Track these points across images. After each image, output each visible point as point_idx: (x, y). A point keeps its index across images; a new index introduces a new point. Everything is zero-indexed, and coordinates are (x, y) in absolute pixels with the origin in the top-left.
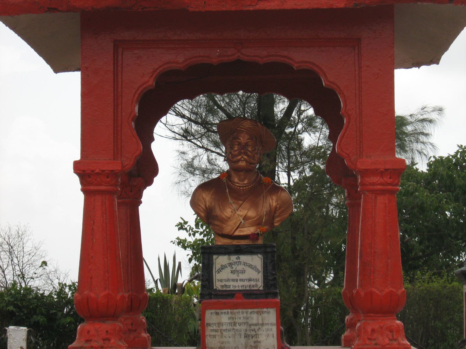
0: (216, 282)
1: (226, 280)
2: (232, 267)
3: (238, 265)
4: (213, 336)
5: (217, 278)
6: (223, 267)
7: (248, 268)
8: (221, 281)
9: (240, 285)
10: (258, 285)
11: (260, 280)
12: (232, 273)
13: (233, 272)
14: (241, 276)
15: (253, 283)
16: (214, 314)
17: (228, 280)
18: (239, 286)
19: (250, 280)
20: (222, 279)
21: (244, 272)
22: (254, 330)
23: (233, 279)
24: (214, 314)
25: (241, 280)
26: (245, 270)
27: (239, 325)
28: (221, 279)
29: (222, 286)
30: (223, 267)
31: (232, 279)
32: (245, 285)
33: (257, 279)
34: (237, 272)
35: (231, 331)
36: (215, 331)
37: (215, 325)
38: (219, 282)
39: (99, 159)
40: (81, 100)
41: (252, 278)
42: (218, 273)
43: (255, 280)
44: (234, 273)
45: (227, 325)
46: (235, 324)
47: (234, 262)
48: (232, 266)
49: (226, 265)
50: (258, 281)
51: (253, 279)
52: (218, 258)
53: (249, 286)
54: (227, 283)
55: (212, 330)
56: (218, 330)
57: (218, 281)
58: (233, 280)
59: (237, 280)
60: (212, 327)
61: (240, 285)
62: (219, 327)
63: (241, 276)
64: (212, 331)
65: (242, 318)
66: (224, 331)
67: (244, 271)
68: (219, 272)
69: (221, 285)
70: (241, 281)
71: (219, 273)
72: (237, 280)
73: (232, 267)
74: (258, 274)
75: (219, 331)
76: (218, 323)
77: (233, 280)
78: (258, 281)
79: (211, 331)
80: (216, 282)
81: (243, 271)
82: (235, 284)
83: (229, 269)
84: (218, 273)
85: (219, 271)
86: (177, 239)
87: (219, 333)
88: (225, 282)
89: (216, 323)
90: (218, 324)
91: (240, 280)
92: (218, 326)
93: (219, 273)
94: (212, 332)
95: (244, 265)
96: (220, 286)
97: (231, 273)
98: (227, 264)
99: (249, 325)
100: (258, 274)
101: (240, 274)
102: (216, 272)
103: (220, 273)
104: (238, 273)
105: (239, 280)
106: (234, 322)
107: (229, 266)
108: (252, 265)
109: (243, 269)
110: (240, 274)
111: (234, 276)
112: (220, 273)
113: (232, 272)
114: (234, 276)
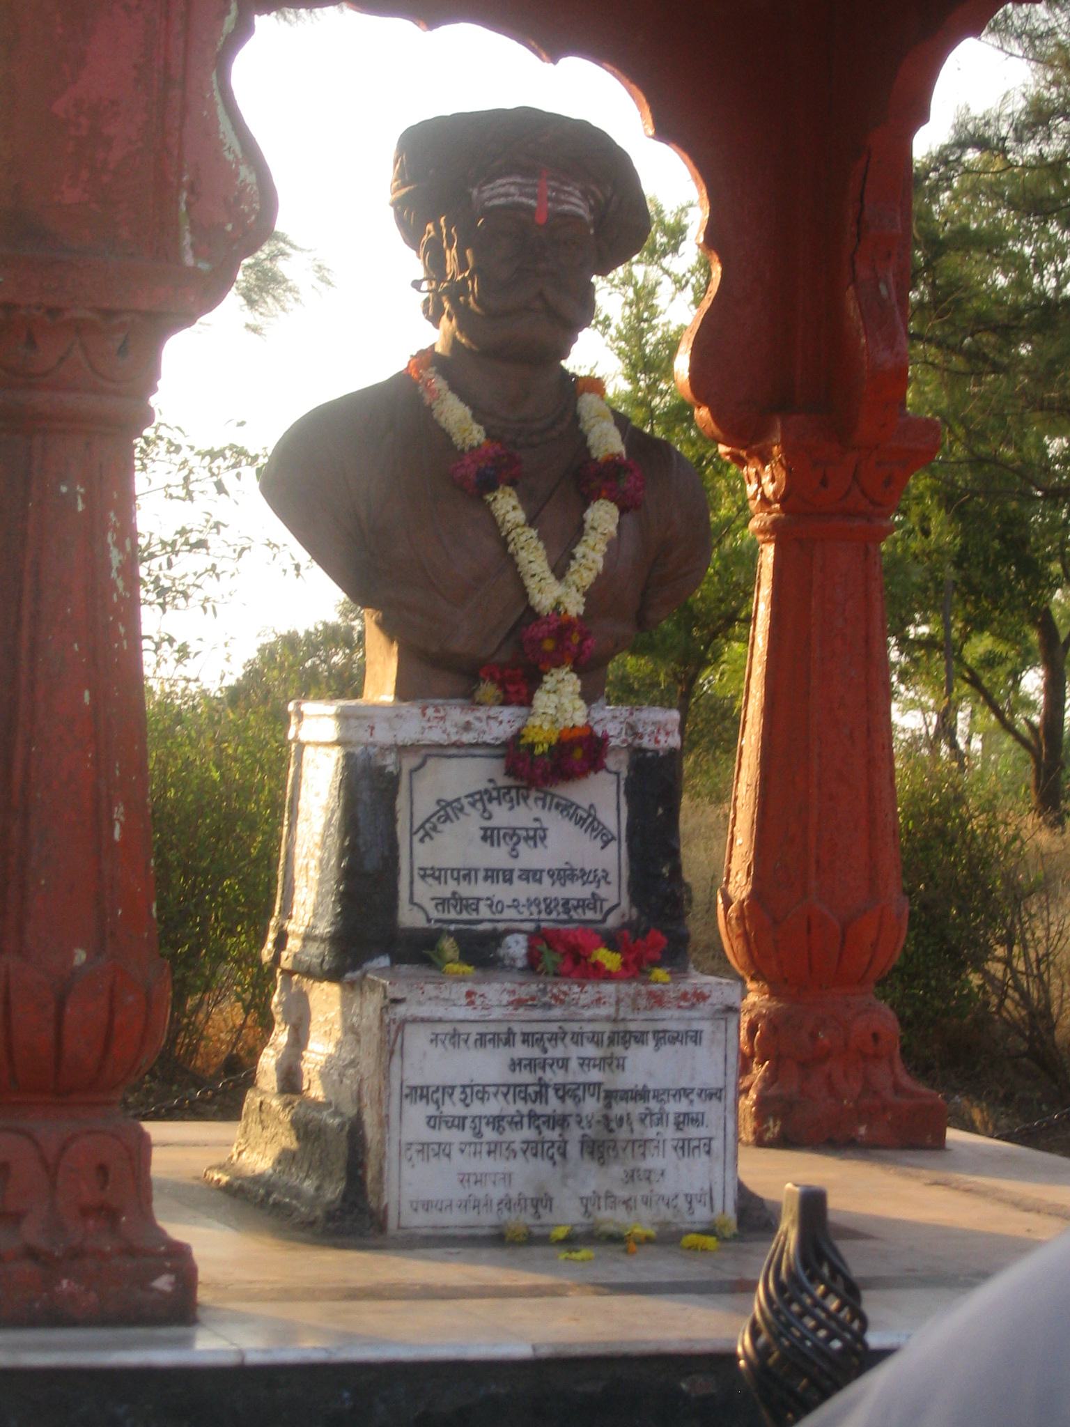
0: (412, 883)
1: (459, 870)
2: (485, 810)
3: (515, 802)
4: (436, 1147)
5: (417, 864)
6: (448, 810)
7: (560, 817)
8: (438, 879)
9: (523, 900)
10: (603, 900)
11: (613, 877)
12: (489, 841)
13: (492, 832)
14: (530, 857)
15: (576, 891)
16: (447, 1042)
17: (467, 875)
18: (515, 904)
19: (564, 875)
20: (440, 870)
21: (543, 838)
22: (625, 1118)
23: (493, 870)
24: (447, 1042)
25: (531, 875)
26: (544, 830)
27: (561, 1093)
28: (437, 866)
29: (442, 903)
30: (448, 810)
31: (487, 870)
32: (545, 900)
33: (600, 874)
34: (511, 839)
35: (521, 1122)
36: (447, 1122)
37: (451, 1095)
38: (430, 880)
39: (818, 862)
40: (376, 385)
41: (577, 864)
42: (422, 840)
43: (591, 878)
44: (495, 838)
45: (505, 1095)
46: (541, 1096)
47: (498, 789)
48: (489, 807)
49: (458, 800)
50: (602, 882)
51: (582, 870)
52: (422, 771)
53: (561, 902)
54: (466, 890)
55: (435, 1117)
56: (464, 1118)
57: (423, 877)
58: (492, 875)
59: (507, 876)
60: (437, 1102)
61: (523, 900)
62: (467, 1106)
63: (530, 857)
64: (432, 1123)
65: (574, 1064)
66: (488, 1124)
67: (540, 833)
68: (427, 834)
69: (438, 895)
70: (527, 879)
71: (427, 839)
72: (507, 876)
73: (485, 810)
74: (603, 848)
75: (468, 1122)
76: (464, 1087)
77: (492, 875)
78: (602, 882)
79: (428, 1123)
80: (412, 883)
81: (536, 830)
82: (501, 891)
83: (472, 822)
84: (422, 840)
85: (427, 831)
86: (604, 871)
87: (467, 1135)
88: (455, 883)
89: (453, 1088)
90: (463, 1092)
91: (520, 877)
92: (463, 1101)
93: (427, 839)
94: (434, 1127)
95: (540, 803)
96: (433, 899)
97: (484, 838)
98: (467, 797)
99: (602, 1095)
100: (603, 848)
101: (522, 847)
102: (416, 833)
103: (432, 838)
104: (515, 839)
105: (516, 874)
106: (536, 1081)
107: (473, 805)
108: (578, 807)
109: (537, 825)
110: (522, 847)
111: (498, 857)
112: (432, 838)
113: (489, 836)
114: (498, 857)
